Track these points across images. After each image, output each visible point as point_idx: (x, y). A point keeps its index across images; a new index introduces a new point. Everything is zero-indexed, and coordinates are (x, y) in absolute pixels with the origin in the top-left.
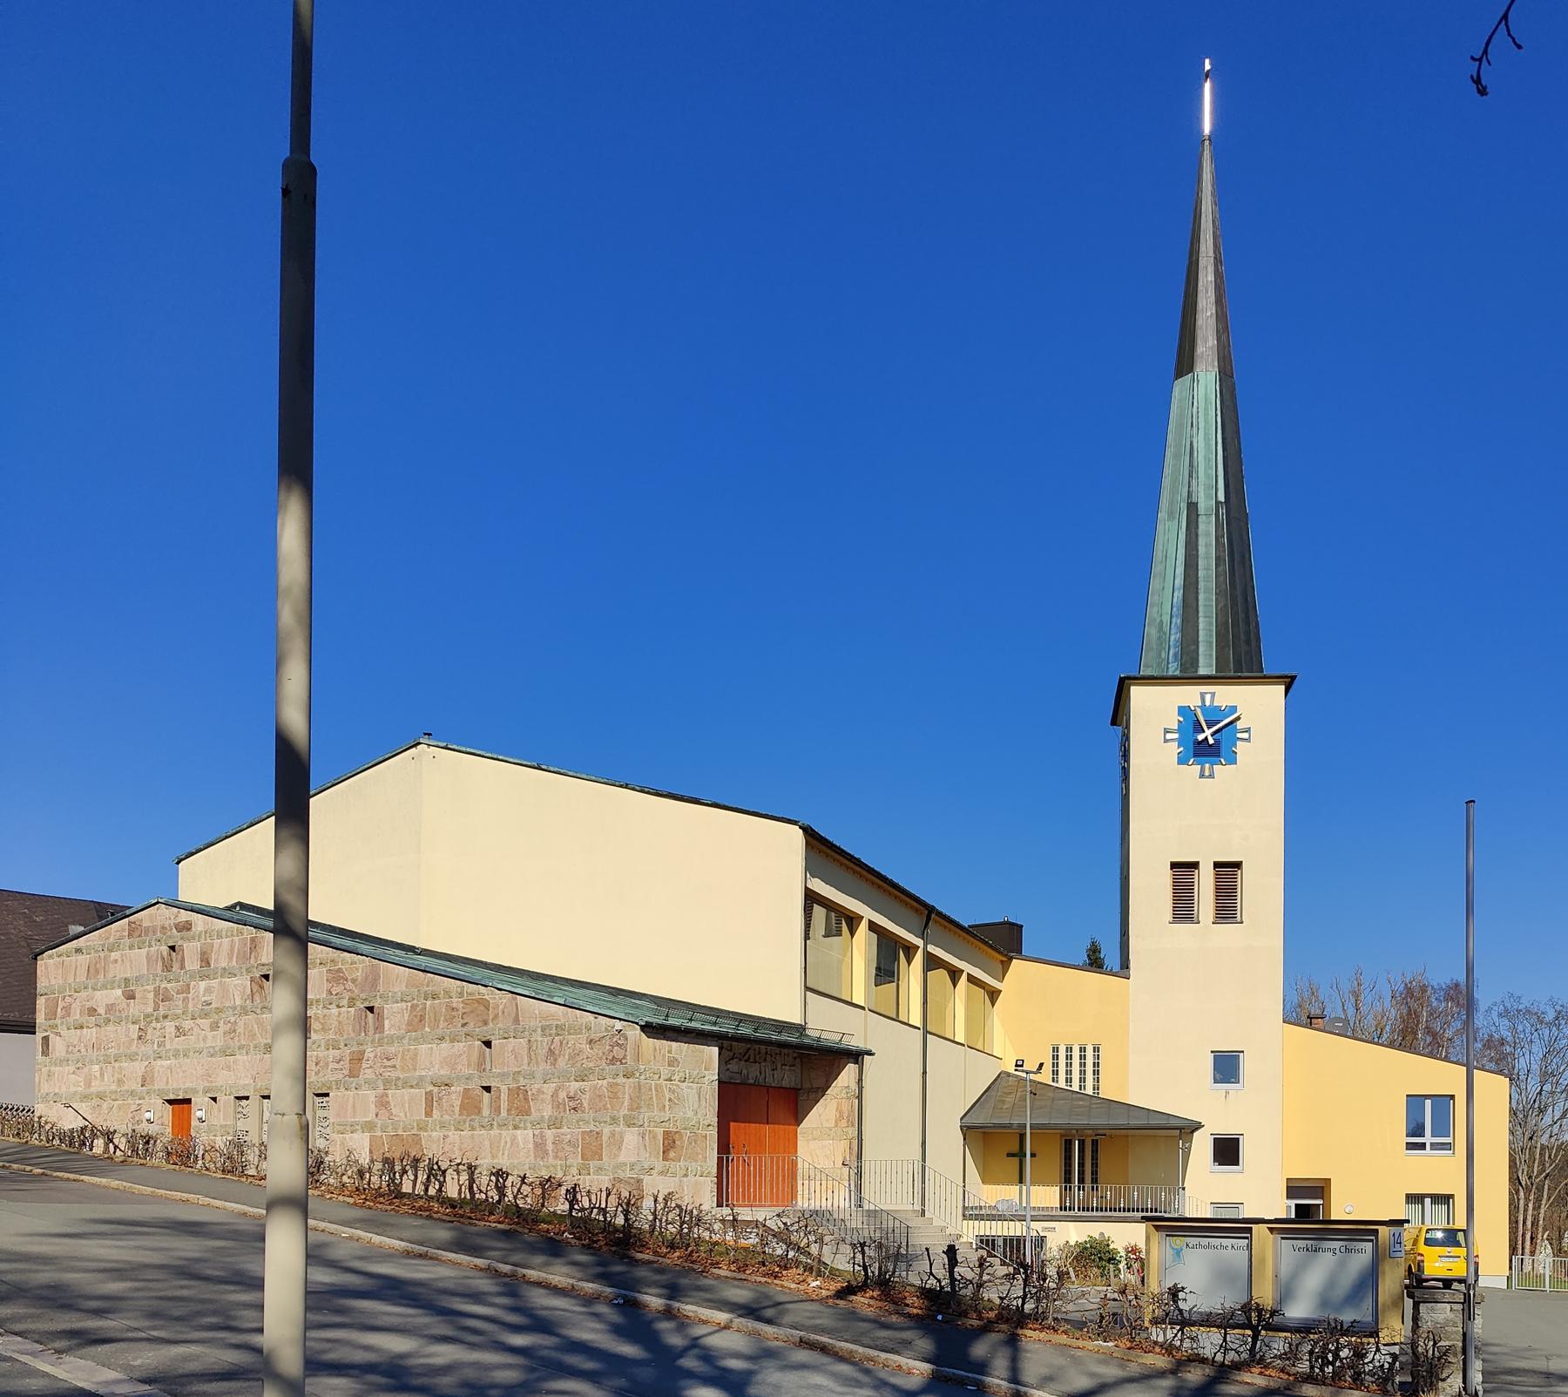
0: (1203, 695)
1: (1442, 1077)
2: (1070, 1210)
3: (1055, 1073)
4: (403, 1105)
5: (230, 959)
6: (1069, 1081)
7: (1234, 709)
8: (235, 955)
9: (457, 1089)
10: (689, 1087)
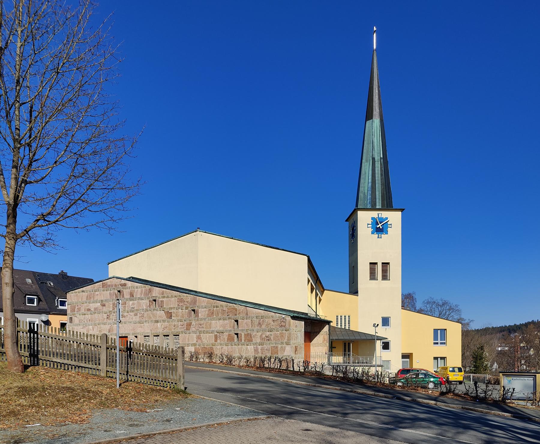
1: (441, 324)
2: (346, 363)
3: (337, 323)
4: (206, 339)
5: (141, 295)
6: (341, 326)
7: (387, 218)
8: (143, 294)
9: (226, 334)
10: (299, 333)
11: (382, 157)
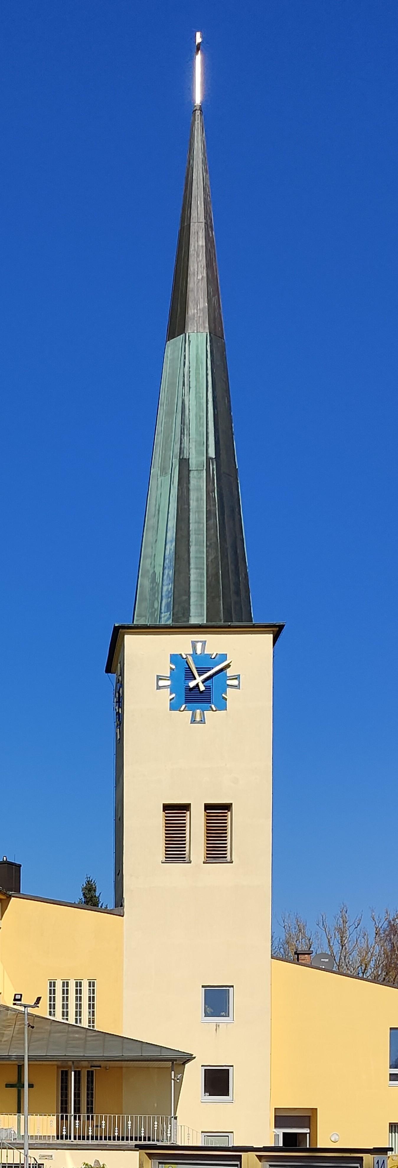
0: (194, 644)
6: (65, 1014)
11: (214, 457)
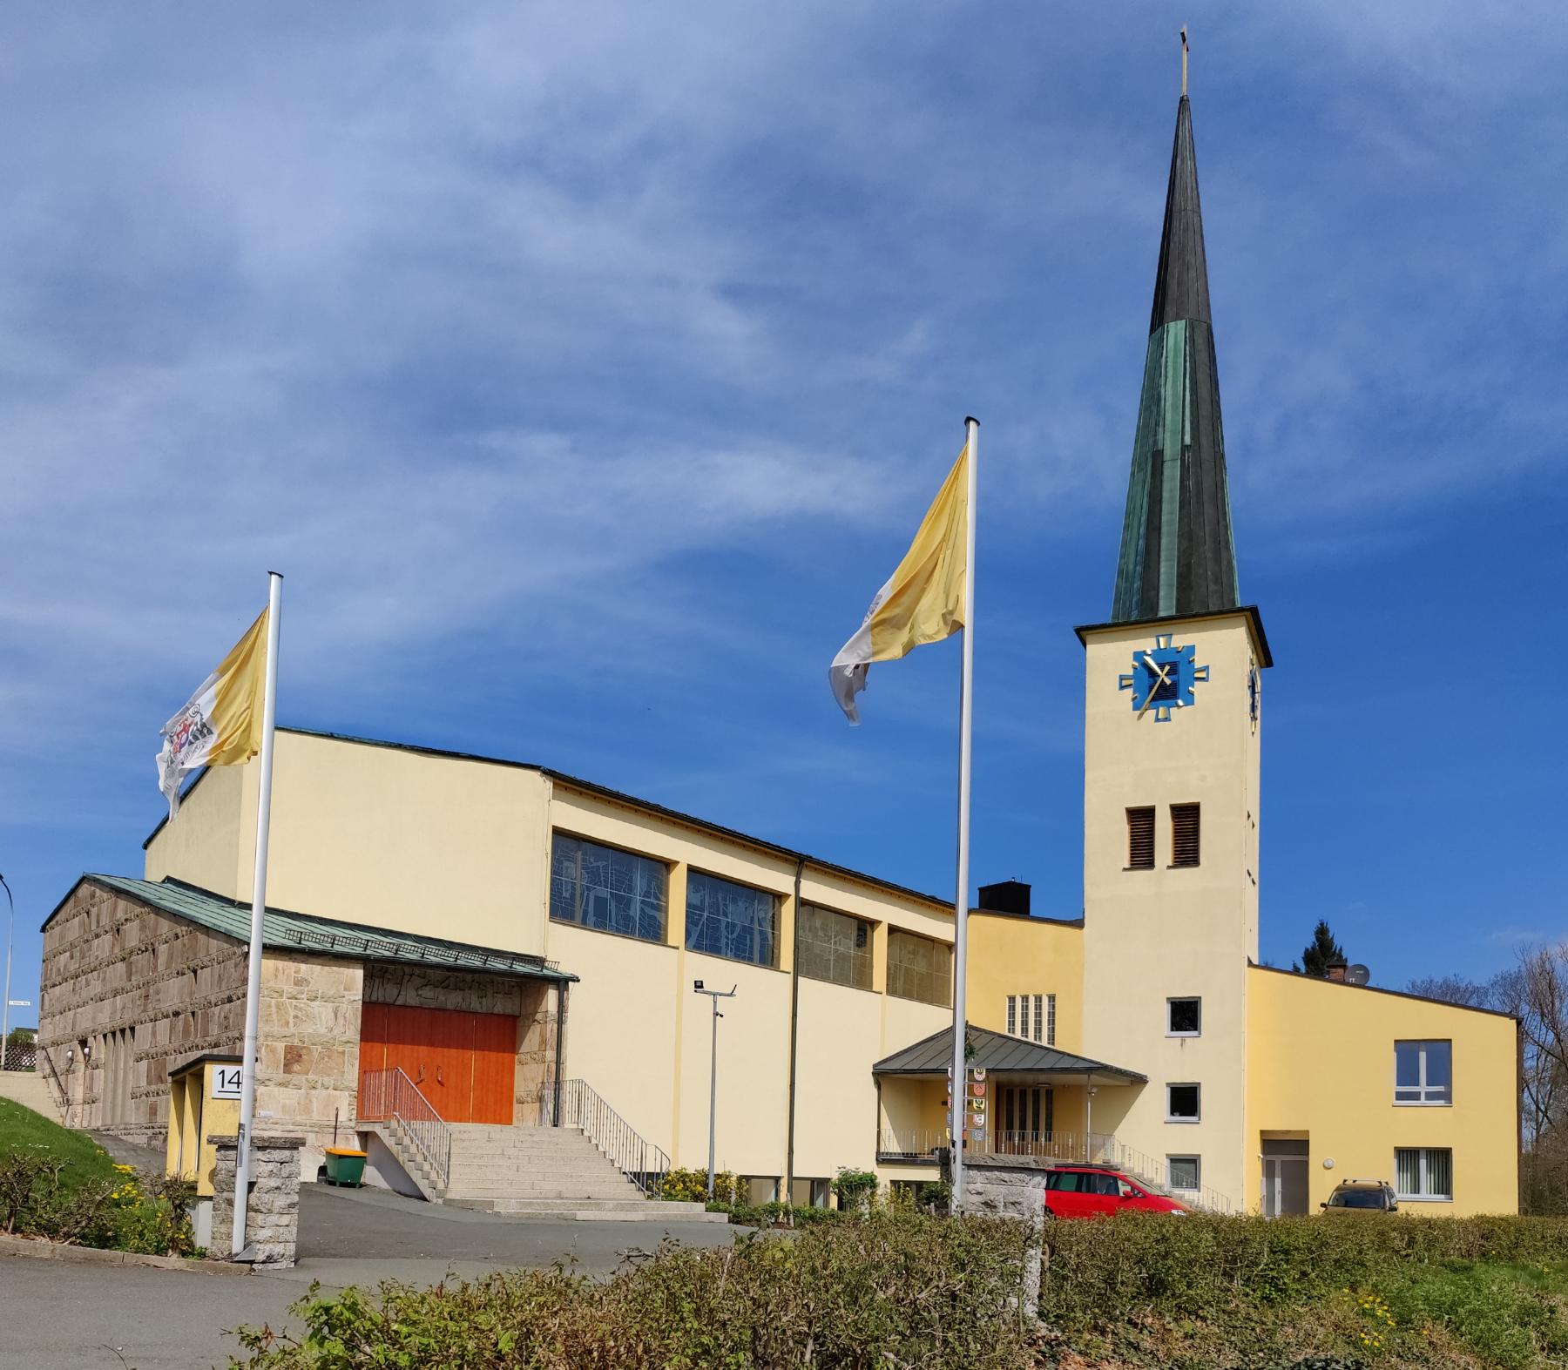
6: (1025, 1030)
